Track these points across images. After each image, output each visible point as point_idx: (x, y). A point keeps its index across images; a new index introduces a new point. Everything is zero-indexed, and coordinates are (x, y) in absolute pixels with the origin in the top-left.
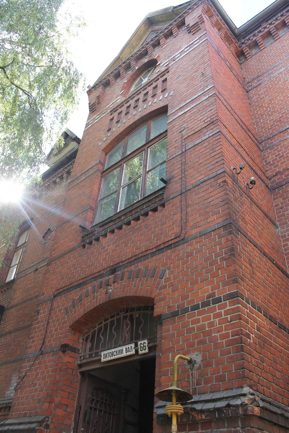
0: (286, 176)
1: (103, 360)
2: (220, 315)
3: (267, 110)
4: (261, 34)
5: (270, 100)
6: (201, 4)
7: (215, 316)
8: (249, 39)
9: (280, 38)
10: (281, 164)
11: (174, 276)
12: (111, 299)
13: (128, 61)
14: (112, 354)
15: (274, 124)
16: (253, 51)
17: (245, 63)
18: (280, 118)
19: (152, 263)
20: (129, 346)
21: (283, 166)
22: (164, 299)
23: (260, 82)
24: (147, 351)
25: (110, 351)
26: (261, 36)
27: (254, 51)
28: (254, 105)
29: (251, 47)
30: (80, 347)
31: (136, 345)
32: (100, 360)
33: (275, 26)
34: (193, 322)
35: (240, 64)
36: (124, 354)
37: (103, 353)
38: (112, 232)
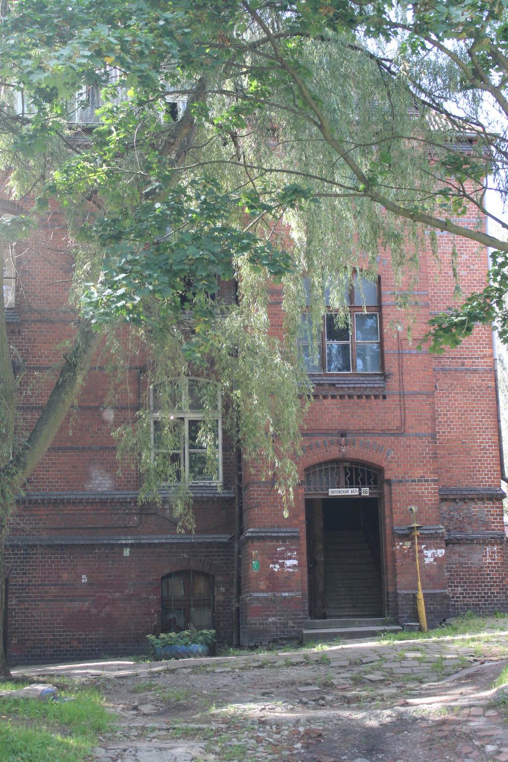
1: (330, 494)
2: (427, 489)
14: (339, 492)
19: (380, 441)
22: (391, 470)
31: (360, 490)
34: (412, 489)
36: (350, 493)
37: (330, 490)
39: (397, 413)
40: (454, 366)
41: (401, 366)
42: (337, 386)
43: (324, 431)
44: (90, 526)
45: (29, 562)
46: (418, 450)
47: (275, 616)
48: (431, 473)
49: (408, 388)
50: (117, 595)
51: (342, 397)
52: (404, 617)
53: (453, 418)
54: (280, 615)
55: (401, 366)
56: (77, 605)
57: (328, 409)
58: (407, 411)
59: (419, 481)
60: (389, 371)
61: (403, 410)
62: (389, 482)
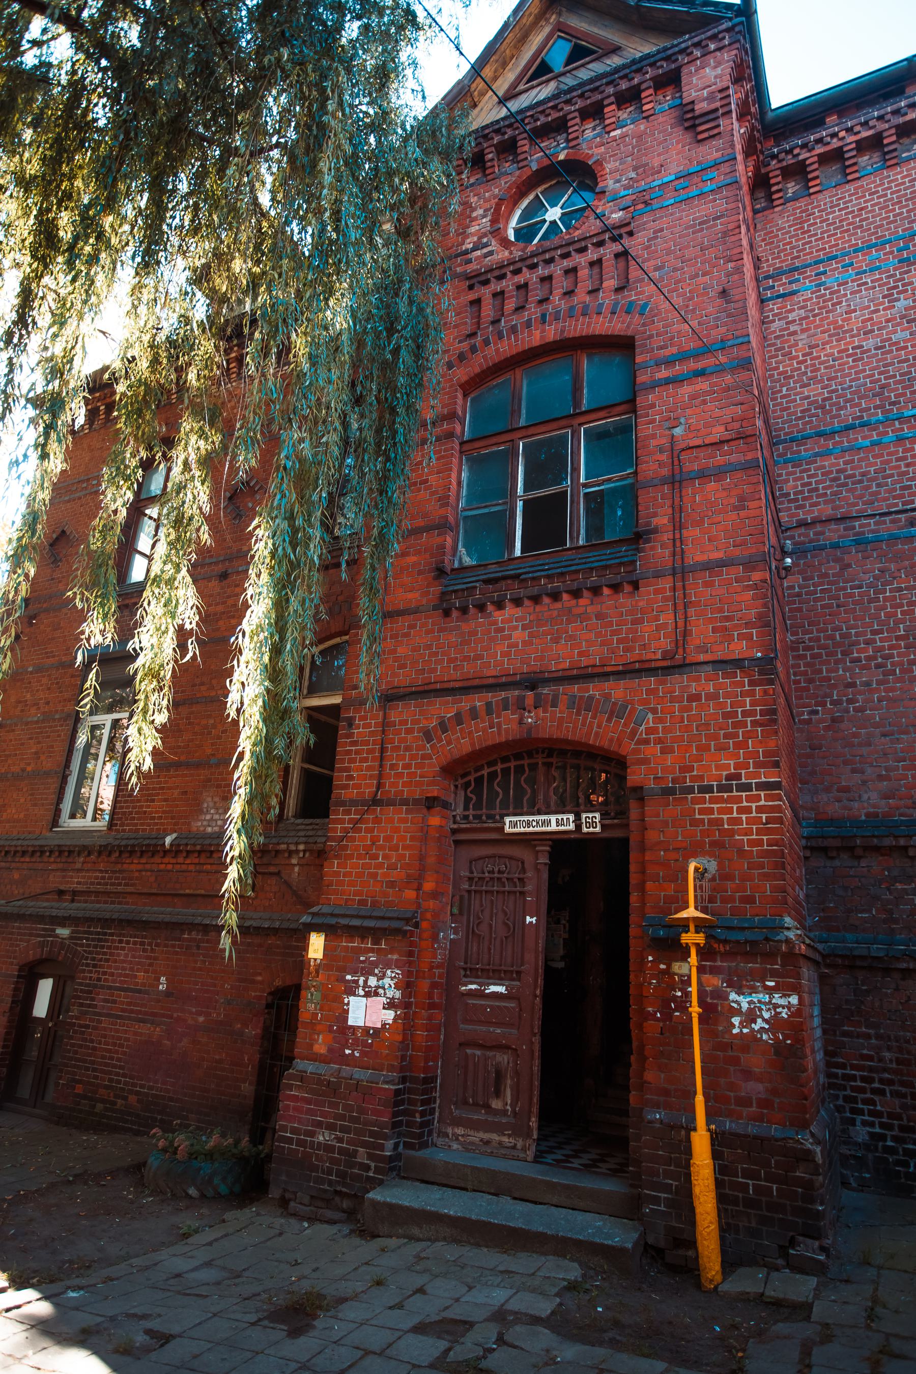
0: (815, 534)
1: (507, 829)
3: (800, 369)
4: (820, 149)
5: (810, 347)
6: (730, 45)
7: (741, 810)
8: (790, 152)
9: (858, 178)
10: (811, 505)
11: (664, 728)
12: (533, 736)
13: (510, 133)
14: (529, 824)
15: (809, 410)
16: (789, 185)
17: (765, 213)
18: (824, 400)
19: (618, 690)
20: (565, 817)
21: (813, 512)
23: (794, 287)
24: (598, 829)
25: (526, 818)
26: (818, 155)
27: (792, 188)
28: (774, 344)
29: (788, 173)
30: (451, 800)
32: (503, 828)
33: (856, 142)
34: (701, 811)
35: (755, 212)
36: (553, 827)
37: (507, 820)
38: (517, 602)
39: (667, 618)
40: (888, 529)
41: (677, 510)
42: (523, 577)
43: (491, 681)
44: (187, 891)
45: (103, 947)
46: (722, 705)
47: (331, 1127)
48: (758, 765)
49: (695, 556)
50: (201, 1019)
51: (536, 599)
52: (656, 1200)
53: (891, 647)
54: (344, 1130)
55: (677, 510)
56: (145, 1029)
57: (503, 630)
58: (692, 611)
59: (721, 788)
60: (648, 524)
61: (681, 611)
62: (639, 792)
